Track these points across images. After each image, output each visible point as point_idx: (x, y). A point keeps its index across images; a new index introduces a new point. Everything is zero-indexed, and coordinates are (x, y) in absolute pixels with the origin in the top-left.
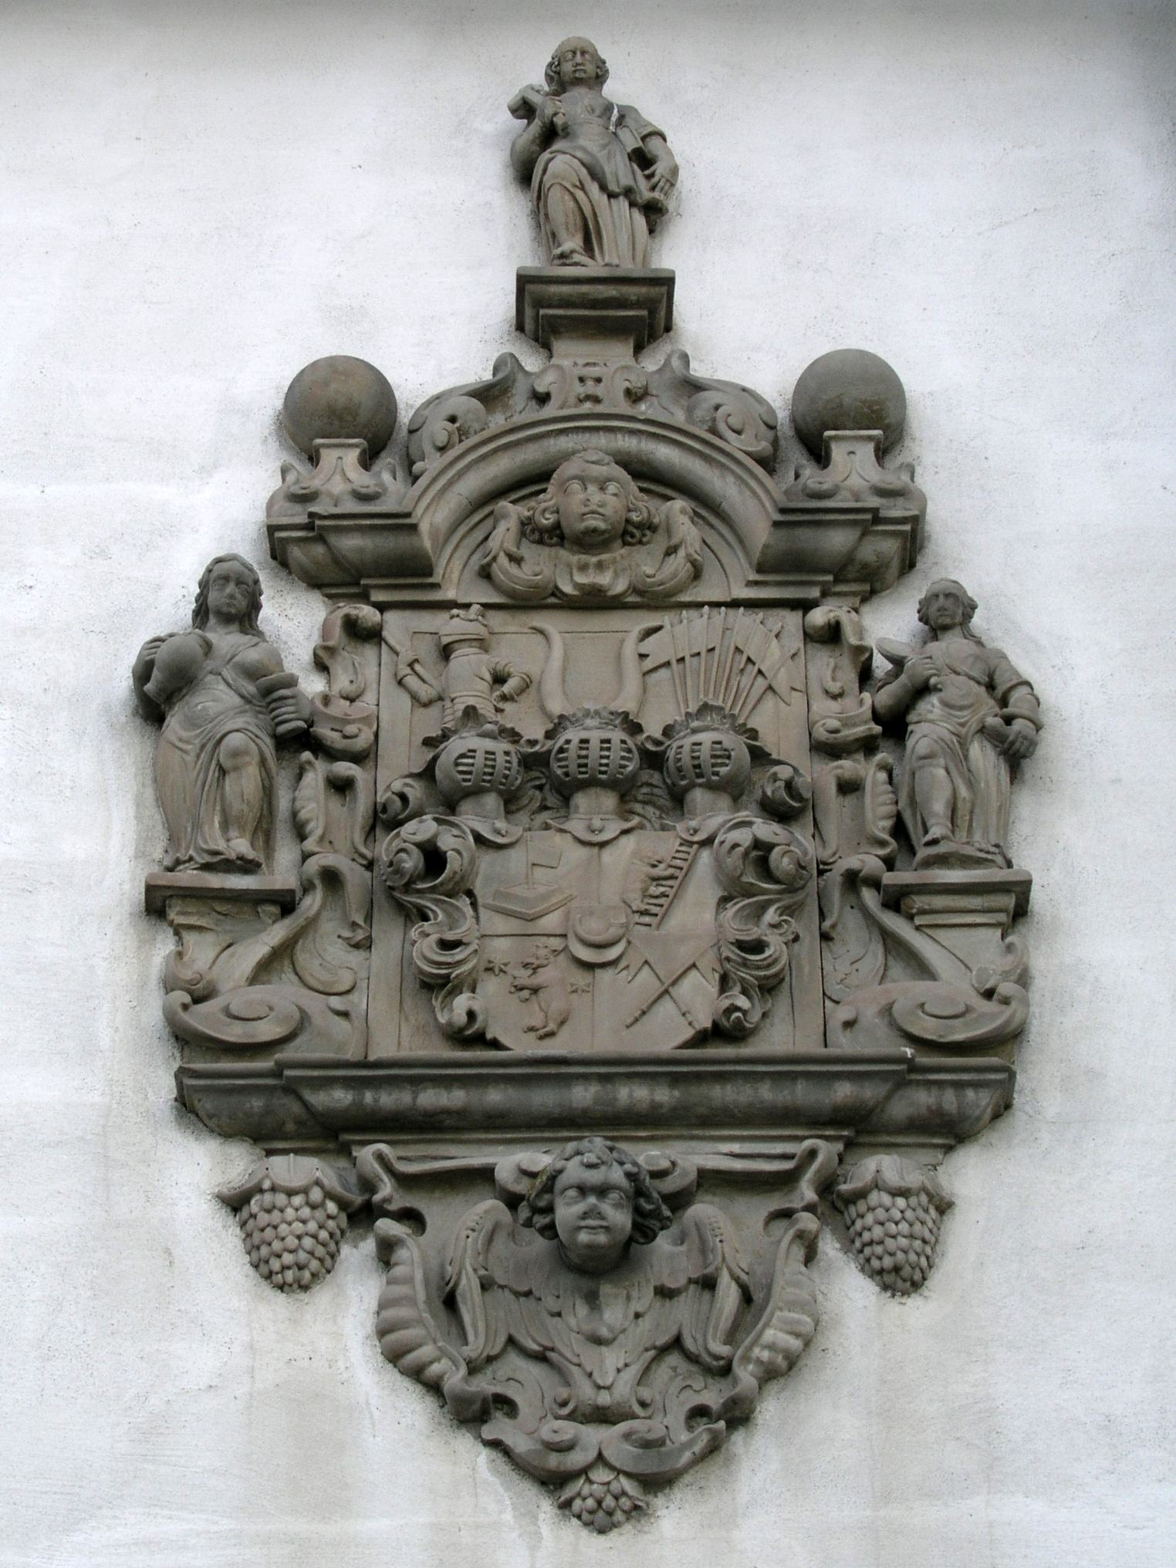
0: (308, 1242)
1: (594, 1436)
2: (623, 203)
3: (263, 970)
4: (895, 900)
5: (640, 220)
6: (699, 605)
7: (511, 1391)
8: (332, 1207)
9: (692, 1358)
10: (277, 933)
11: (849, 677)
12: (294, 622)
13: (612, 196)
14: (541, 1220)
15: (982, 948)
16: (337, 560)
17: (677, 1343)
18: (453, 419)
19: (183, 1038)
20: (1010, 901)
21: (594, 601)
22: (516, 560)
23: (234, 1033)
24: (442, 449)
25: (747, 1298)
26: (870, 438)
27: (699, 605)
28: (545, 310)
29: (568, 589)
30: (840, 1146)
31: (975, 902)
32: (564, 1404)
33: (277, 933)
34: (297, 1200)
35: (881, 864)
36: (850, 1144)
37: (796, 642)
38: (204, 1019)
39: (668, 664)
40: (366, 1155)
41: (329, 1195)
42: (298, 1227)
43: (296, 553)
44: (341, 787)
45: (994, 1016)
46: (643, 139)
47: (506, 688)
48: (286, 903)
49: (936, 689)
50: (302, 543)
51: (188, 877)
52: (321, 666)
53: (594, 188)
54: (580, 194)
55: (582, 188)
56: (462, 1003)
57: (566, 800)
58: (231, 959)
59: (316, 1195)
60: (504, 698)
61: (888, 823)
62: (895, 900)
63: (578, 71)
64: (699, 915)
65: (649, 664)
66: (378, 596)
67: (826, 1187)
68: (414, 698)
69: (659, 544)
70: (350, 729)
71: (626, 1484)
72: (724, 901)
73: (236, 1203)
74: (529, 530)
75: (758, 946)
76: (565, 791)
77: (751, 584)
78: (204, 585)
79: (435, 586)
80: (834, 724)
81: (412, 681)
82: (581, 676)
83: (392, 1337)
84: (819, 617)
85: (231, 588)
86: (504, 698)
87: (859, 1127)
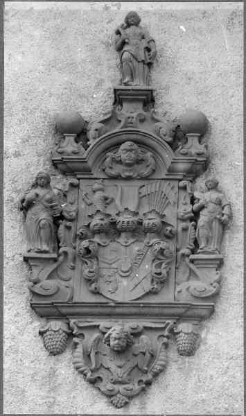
0: (59, 343)
1: (116, 387)
2: (141, 64)
3: (50, 277)
4: (192, 261)
5: (146, 67)
6: (154, 179)
7: (101, 376)
8: (64, 334)
9: (140, 369)
10: (55, 265)
11: (188, 200)
12: (60, 183)
13: (139, 62)
14: (107, 343)
15: (213, 275)
16: (69, 168)
17: (137, 366)
18: (96, 130)
19: (34, 294)
20: (218, 262)
21: (129, 178)
22: (111, 168)
23: (44, 293)
24: (94, 138)
25: (152, 356)
26: (196, 136)
27: (154, 179)
28: (120, 97)
29: (123, 176)
30: (175, 321)
31: (210, 262)
32: (112, 380)
33: (55, 265)
34: (57, 333)
35: (190, 252)
36: (178, 320)
37: (176, 189)
38: (37, 289)
39: (145, 196)
40: (72, 321)
41: (64, 331)
42: (56, 339)
43: (59, 166)
44: (69, 228)
45: (210, 291)
46: (148, 43)
47: (108, 201)
48: (55, 260)
49: (206, 207)
50: (62, 166)
51: (33, 254)
52: (41, 287)
53: (134, 61)
54: (130, 64)
55: (131, 62)
56: (93, 285)
57: (120, 234)
58: (41, 272)
59: (61, 332)
60: (108, 204)
61: (193, 241)
62: (192, 261)
63: (132, 21)
64: (147, 267)
65: (141, 196)
66: (78, 176)
67: (171, 331)
68: (86, 203)
69: (144, 165)
70: (71, 214)
71: (124, 397)
72: (153, 261)
73: (41, 333)
74: (113, 160)
75: (160, 274)
76: (119, 233)
77: (166, 175)
78: (37, 179)
79: (92, 174)
80: (182, 214)
81: (86, 199)
82: (127, 201)
83: (76, 365)
84: (181, 184)
85: (43, 180)
86: (108, 204)
87: (180, 318)
